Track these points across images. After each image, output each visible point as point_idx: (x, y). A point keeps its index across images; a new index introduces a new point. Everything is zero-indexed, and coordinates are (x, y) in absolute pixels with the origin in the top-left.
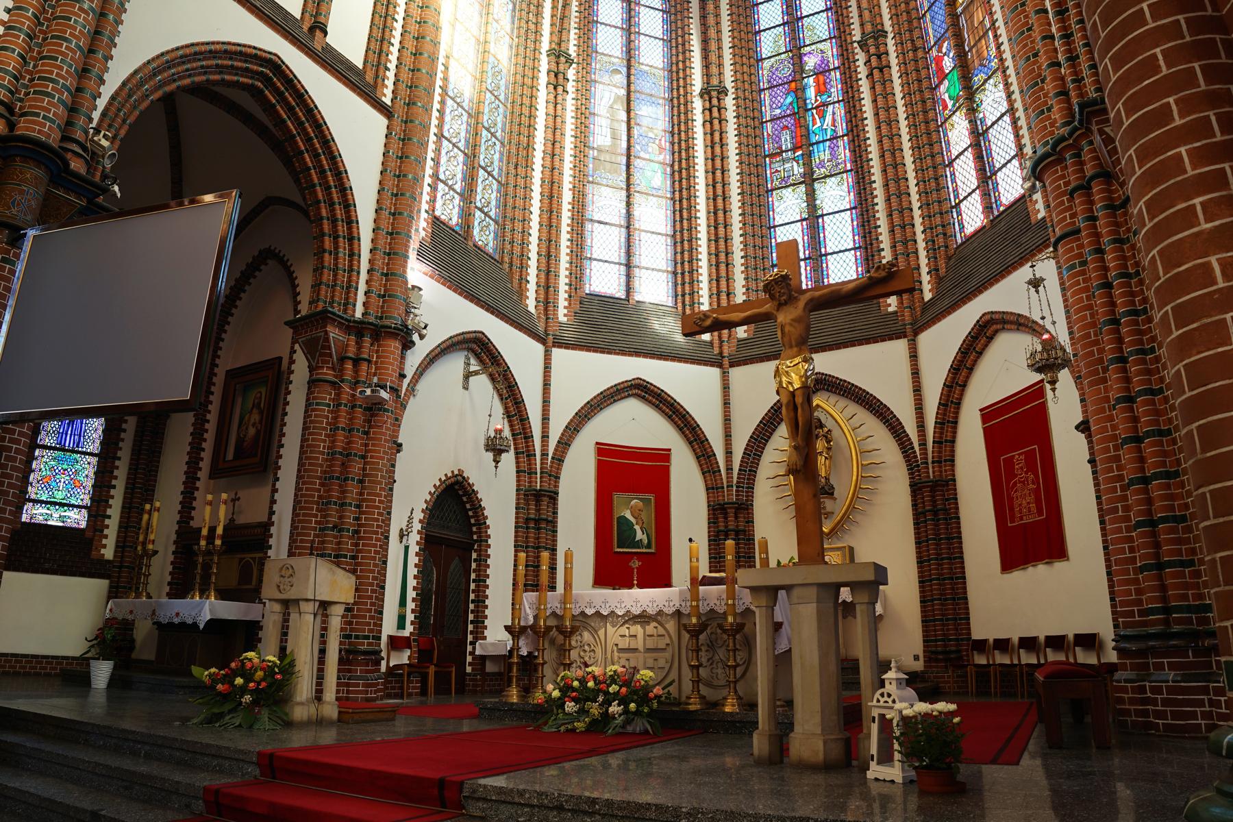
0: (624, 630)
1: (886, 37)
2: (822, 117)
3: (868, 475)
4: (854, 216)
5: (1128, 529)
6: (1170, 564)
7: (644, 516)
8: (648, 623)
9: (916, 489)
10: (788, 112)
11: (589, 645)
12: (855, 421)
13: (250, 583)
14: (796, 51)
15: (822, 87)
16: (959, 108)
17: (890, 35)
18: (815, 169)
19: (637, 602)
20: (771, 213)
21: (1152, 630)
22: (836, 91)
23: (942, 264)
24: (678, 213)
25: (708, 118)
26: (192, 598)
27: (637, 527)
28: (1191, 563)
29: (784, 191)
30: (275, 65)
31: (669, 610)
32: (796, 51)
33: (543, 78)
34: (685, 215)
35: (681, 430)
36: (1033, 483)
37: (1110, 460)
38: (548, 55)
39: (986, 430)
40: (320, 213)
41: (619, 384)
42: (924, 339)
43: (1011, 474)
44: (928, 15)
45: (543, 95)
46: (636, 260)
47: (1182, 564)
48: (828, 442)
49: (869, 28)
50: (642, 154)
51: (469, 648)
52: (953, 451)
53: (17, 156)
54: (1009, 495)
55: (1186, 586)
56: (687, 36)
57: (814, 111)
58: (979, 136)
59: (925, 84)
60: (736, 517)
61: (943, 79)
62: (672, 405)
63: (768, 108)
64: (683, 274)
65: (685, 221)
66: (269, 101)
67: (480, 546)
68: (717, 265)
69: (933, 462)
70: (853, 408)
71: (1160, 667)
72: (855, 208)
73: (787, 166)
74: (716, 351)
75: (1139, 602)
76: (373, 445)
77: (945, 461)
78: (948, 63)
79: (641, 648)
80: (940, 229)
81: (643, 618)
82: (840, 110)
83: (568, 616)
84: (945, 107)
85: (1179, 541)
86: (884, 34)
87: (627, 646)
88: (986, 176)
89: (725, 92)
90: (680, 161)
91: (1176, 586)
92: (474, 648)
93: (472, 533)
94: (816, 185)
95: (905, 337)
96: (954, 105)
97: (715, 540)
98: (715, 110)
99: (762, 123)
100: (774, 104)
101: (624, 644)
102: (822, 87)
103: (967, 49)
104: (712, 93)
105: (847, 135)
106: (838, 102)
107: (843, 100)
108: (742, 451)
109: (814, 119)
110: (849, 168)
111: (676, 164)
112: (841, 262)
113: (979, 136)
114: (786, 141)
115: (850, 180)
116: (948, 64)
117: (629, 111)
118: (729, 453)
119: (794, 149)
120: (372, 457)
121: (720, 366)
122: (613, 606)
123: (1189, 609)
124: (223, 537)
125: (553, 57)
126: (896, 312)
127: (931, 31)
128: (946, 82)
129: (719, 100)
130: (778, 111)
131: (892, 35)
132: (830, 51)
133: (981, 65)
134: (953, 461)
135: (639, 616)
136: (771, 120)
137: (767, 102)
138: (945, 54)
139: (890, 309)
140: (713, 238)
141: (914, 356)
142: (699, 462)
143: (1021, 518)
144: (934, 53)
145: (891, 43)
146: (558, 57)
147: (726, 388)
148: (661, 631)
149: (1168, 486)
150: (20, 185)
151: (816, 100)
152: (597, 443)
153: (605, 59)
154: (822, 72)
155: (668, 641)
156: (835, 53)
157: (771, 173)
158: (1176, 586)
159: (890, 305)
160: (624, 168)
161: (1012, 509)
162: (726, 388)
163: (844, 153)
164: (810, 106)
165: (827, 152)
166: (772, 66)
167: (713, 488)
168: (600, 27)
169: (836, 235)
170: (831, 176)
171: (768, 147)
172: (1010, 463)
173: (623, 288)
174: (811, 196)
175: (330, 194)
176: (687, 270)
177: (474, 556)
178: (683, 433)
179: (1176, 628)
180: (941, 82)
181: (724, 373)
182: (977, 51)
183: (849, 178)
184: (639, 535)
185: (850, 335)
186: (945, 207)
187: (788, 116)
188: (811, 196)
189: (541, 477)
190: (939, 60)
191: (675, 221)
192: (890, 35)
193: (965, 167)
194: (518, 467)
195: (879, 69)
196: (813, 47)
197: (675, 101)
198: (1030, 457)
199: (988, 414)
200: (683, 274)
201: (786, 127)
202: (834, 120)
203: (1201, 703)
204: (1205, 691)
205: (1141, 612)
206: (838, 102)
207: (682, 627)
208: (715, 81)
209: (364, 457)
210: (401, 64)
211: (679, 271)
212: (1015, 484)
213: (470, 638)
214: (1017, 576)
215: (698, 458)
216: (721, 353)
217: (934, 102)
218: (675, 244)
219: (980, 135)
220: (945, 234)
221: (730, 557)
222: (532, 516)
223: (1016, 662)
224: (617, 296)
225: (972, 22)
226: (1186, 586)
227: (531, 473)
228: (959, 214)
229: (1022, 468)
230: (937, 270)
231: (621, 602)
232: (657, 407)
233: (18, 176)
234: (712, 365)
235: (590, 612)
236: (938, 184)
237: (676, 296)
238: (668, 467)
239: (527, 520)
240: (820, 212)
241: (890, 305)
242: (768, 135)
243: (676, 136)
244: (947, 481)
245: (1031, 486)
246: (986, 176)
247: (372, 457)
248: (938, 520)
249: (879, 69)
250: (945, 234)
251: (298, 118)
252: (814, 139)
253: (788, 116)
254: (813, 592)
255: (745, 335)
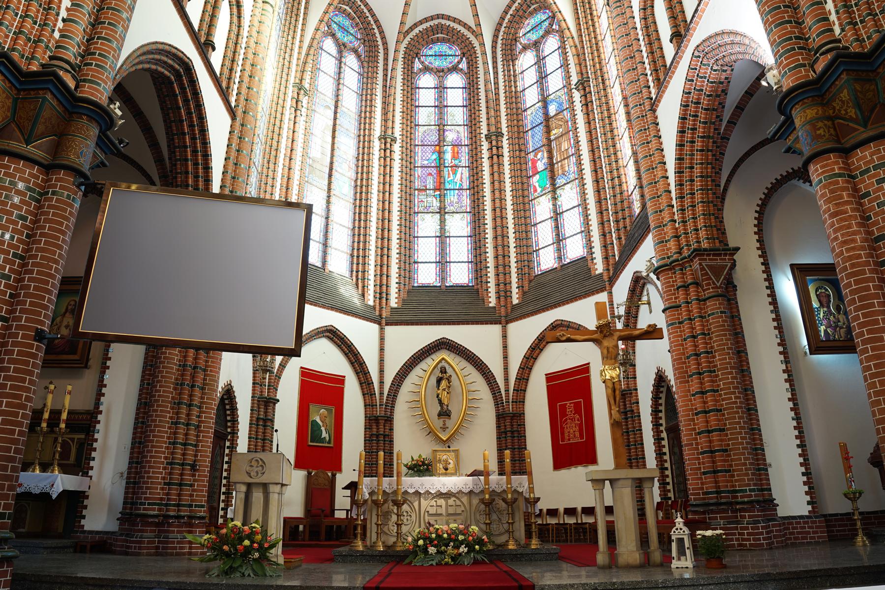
0: (433, 503)
1: (503, 137)
2: (454, 173)
3: (472, 405)
4: (470, 241)
5: (698, 454)
6: (721, 471)
7: (327, 420)
8: (450, 498)
9: (500, 417)
10: (433, 165)
11: (407, 512)
12: (466, 372)
13: (68, 459)
14: (441, 127)
15: (456, 154)
16: (545, 194)
17: (505, 137)
18: (447, 206)
19: (444, 485)
20: (416, 228)
21: (711, 501)
22: (464, 159)
23: (526, 284)
24: (357, 214)
25: (383, 155)
26: (34, 471)
27: (323, 429)
28: (729, 471)
29: (426, 215)
30: (188, 68)
31: (466, 491)
32: (441, 127)
33: (288, 103)
34: (363, 217)
35: (352, 363)
36: (578, 420)
37: (690, 420)
38: (293, 86)
39: (548, 387)
40: (187, 181)
41: (319, 328)
42: (512, 327)
43: (564, 413)
44: (530, 132)
45: (288, 114)
46: (330, 242)
47: (726, 471)
48: (449, 383)
49: (493, 129)
50: (338, 169)
51: (221, 513)
52: (524, 396)
53: (85, 115)
54: (561, 426)
55: (728, 481)
56: (374, 96)
57: (450, 169)
58: (557, 215)
59: (524, 173)
60: (384, 426)
61: (536, 174)
62: (349, 346)
63: (420, 158)
64: (358, 257)
65: (362, 221)
66: (175, 92)
67: (233, 437)
68: (382, 256)
69: (512, 402)
70: (464, 363)
71: (716, 518)
72: (471, 236)
73: (429, 199)
74: (377, 313)
75: (702, 489)
76: (212, 362)
77: (520, 402)
78: (540, 166)
79: (444, 513)
80: (526, 263)
81: (447, 495)
82: (466, 172)
83: (400, 493)
84: (535, 191)
85: (725, 461)
86: (502, 135)
87: (435, 512)
88: (559, 239)
89: (394, 140)
90: (362, 180)
91: (723, 481)
92: (226, 513)
93: (227, 427)
94: (447, 216)
95: (500, 323)
96: (542, 191)
97: (369, 440)
98: (388, 151)
99: (415, 167)
100: (425, 156)
101: (432, 511)
102: (456, 154)
103: (555, 162)
104: (386, 139)
105: (469, 189)
106: (466, 167)
107: (468, 167)
108: (391, 382)
109: (449, 174)
110: (468, 210)
111: (359, 181)
112: (459, 269)
113: (557, 215)
114: (430, 183)
115: (469, 218)
116: (540, 166)
117: (334, 137)
118: (381, 383)
119: (435, 190)
120: (211, 371)
121: (380, 324)
122: (428, 488)
123: (729, 492)
124: (67, 422)
125: (296, 88)
126: (494, 308)
127: (531, 143)
128: (537, 176)
129: (391, 145)
130: (426, 162)
131: (507, 137)
132: (463, 134)
133: (564, 174)
134: (524, 402)
135: (446, 494)
136: (422, 167)
137: (420, 154)
138: (539, 160)
139: (491, 305)
140: (380, 237)
141: (505, 336)
142: (361, 387)
143: (569, 440)
144: (531, 156)
145: (505, 143)
146: (300, 89)
147: (382, 339)
148: (458, 503)
149: (720, 435)
150: (86, 140)
151: (452, 162)
152: (301, 368)
153: (322, 96)
154: (456, 145)
155: (463, 508)
156: (466, 135)
157: (418, 202)
158: (723, 481)
159: (490, 302)
160: (327, 176)
161: (563, 434)
162: (382, 339)
163: (466, 201)
164: (447, 165)
165: (456, 197)
166: (425, 132)
167: (369, 405)
168: (321, 74)
169: (457, 251)
170: (457, 213)
171: (417, 184)
172: (563, 408)
173: (320, 259)
174: (442, 222)
175: (197, 169)
176: (361, 255)
177: (228, 444)
178: (353, 366)
179: (723, 500)
180: (534, 175)
181: (382, 329)
182: (562, 165)
183: (468, 217)
184: (324, 434)
185: (466, 317)
186: (530, 250)
187: (432, 167)
188: (442, 222)
189: (268, 389)
190: (534, 162)
191: (354, 220)
192: (505, 137)
193: (545, 230)
194: (254, 380)
195: (496, 156)
196: (453, 127)
197: (362, 137)
198: (577, 407)
199: (551, 378)
200: (358, 257)
201: (430, 174)
202: (462, 178)
203: (734, 534)
204: (736, 528)
205: (704, 494)
206: (466, 167)
207: (482, 501)
208: (389, 132)
209: (205, 370)
210: (242, 81)
211: (355, 254)
212: (566, 420)
213: (222, 505)
214: (564, 472)
215: (361, 384)
216: (380, 315)
217: (529, 185)
218: (354, 235)
219: (557, 214)
220: (529, 266)
221: (508, 460)
222: (262, 417)
223: (579, 522)
224: (316, 265)
225: (560, 148)
226: (728, 481)
227: (262, 385)
228: (538, 256)
229: (571, 411)
230: (523, 287)
231: (433, 485)
232: (339, 346)
233: (85, 132)
234: (375, 323)
235: (411, 491)
236: (527, 236)
237: (352, 271)
238: (343, 388)
239: (258, 419)
240: (447, 234)
241: (490, 302)
242: (419, 176)
243: (360, 162)
244: (520, 414)
245: (577, 422)
246: (559, 239)
247: (211, 371)
248: (514, 437)
249: (496, 156)
250: (529, 266)
251: (189, 109)
252: (447, 186)
253: (432, 167)
254: (629, 482)
255: (396, 306)
